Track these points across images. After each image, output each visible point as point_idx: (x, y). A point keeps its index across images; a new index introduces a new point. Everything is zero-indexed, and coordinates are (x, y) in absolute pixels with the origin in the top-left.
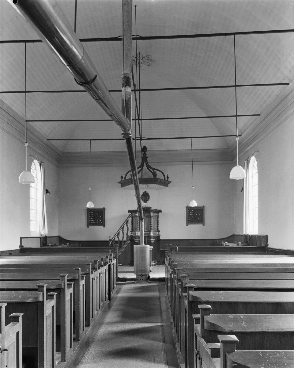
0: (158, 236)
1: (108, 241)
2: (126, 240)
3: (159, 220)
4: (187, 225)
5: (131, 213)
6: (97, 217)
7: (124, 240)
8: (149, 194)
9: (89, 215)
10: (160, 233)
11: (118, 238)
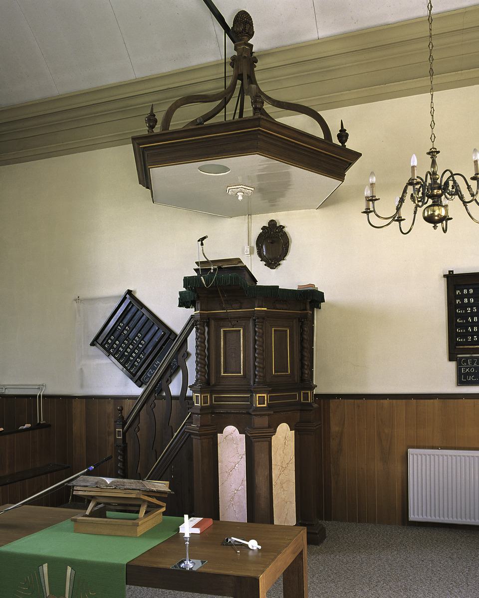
8: (286, 230)
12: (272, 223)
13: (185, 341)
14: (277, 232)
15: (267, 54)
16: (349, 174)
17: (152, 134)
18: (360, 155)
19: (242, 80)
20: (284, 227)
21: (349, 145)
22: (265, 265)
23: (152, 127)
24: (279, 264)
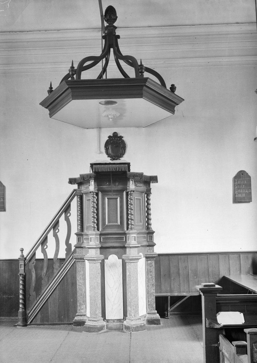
1: (16, 261)
2: (64, 257)
3: (151, 202)
5: (75, 186)
7: (59, 257)
11: (44, 251)
12: (115, 134)
20: (123, 137)
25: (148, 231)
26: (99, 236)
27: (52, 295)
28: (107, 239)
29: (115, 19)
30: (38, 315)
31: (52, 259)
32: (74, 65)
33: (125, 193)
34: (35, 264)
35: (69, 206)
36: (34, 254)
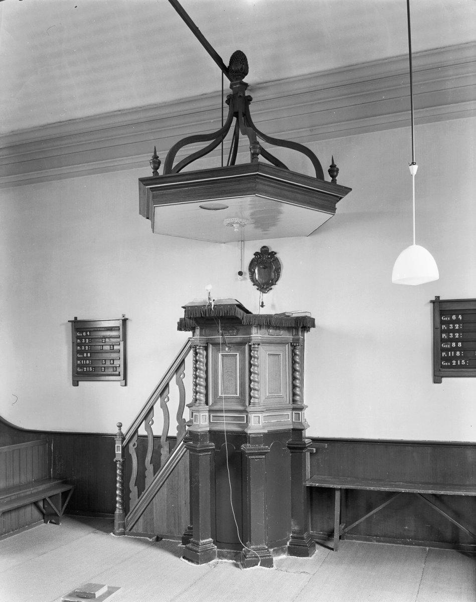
0: (293, 430)
4: (437, 379)
6: (93, 352)
7: (169, 435)
8: (277, 256)
9: (78, 345)
10: (307, 416)
12: (265, 250)
13: (182, 362)
14: (269, 258)
15: (259, 86)
16: (338, 205)
17: (158, 177)
18: (351, 189)
19: (237, 117)
20: (276, 253)
21: (340, 180)
22: (258, 289)
23: (156, 169)
24: (271, 289)
25: (295, 405)
26: (207, 414)
27: (159, 493)
28: (218, 418)
29: (245, 72)
30: (140, 520)
31: (159, 437)
32: (157, 153)
33: (247, 347)
34: (136, 446)
35: (183, 361)
36: (136, 431)
